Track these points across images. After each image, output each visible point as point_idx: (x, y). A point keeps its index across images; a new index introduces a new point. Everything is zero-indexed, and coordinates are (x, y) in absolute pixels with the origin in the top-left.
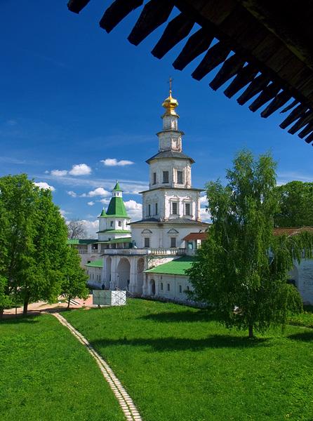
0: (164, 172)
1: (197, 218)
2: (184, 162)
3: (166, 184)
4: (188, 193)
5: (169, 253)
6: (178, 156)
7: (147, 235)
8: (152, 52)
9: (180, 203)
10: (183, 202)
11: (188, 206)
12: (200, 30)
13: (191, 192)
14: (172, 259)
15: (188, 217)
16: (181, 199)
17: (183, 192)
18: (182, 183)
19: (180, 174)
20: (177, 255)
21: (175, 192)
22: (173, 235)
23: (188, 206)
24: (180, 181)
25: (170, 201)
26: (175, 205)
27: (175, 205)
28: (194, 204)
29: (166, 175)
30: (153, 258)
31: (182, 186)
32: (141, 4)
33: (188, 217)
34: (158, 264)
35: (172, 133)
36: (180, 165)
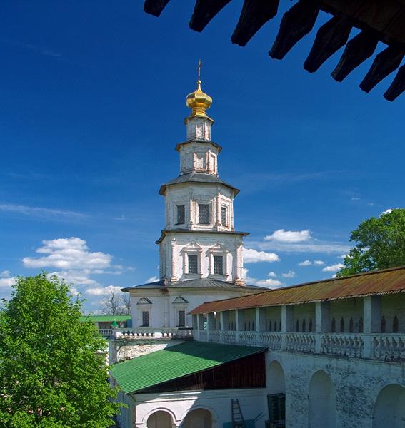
0: (178, 207)
1: (235, 278)
2: (212, 189)
3: (181, 226)
4: (218, 238)
5: (158, 335)
6: (201, 180)
7: (145, 307)
8: (368, 92)
9: (203, 256)
10: (208, 254)
11: (219, 261)
12: (387, 48)
13: (223, 237)
14: (165, 345)
15: (220, 278)
16: (205, 248)
17: (210, 237)
18: (208, 223)
19: (205, 210)
20: (175, 339)
21: (192, 237)
22: (181, 307)
23: (219, 261)
24: (205, 219)
25: (183, 252)
26: (194, 260)
27: (194, 260)
28: (229, 257)
29: (182, 212)
30: (125, 345)
31: (209, 228)
32: (273, 12)
33: (220, 278)
34: (138, 354)
35: (197, 145)
36: (205, 193)
